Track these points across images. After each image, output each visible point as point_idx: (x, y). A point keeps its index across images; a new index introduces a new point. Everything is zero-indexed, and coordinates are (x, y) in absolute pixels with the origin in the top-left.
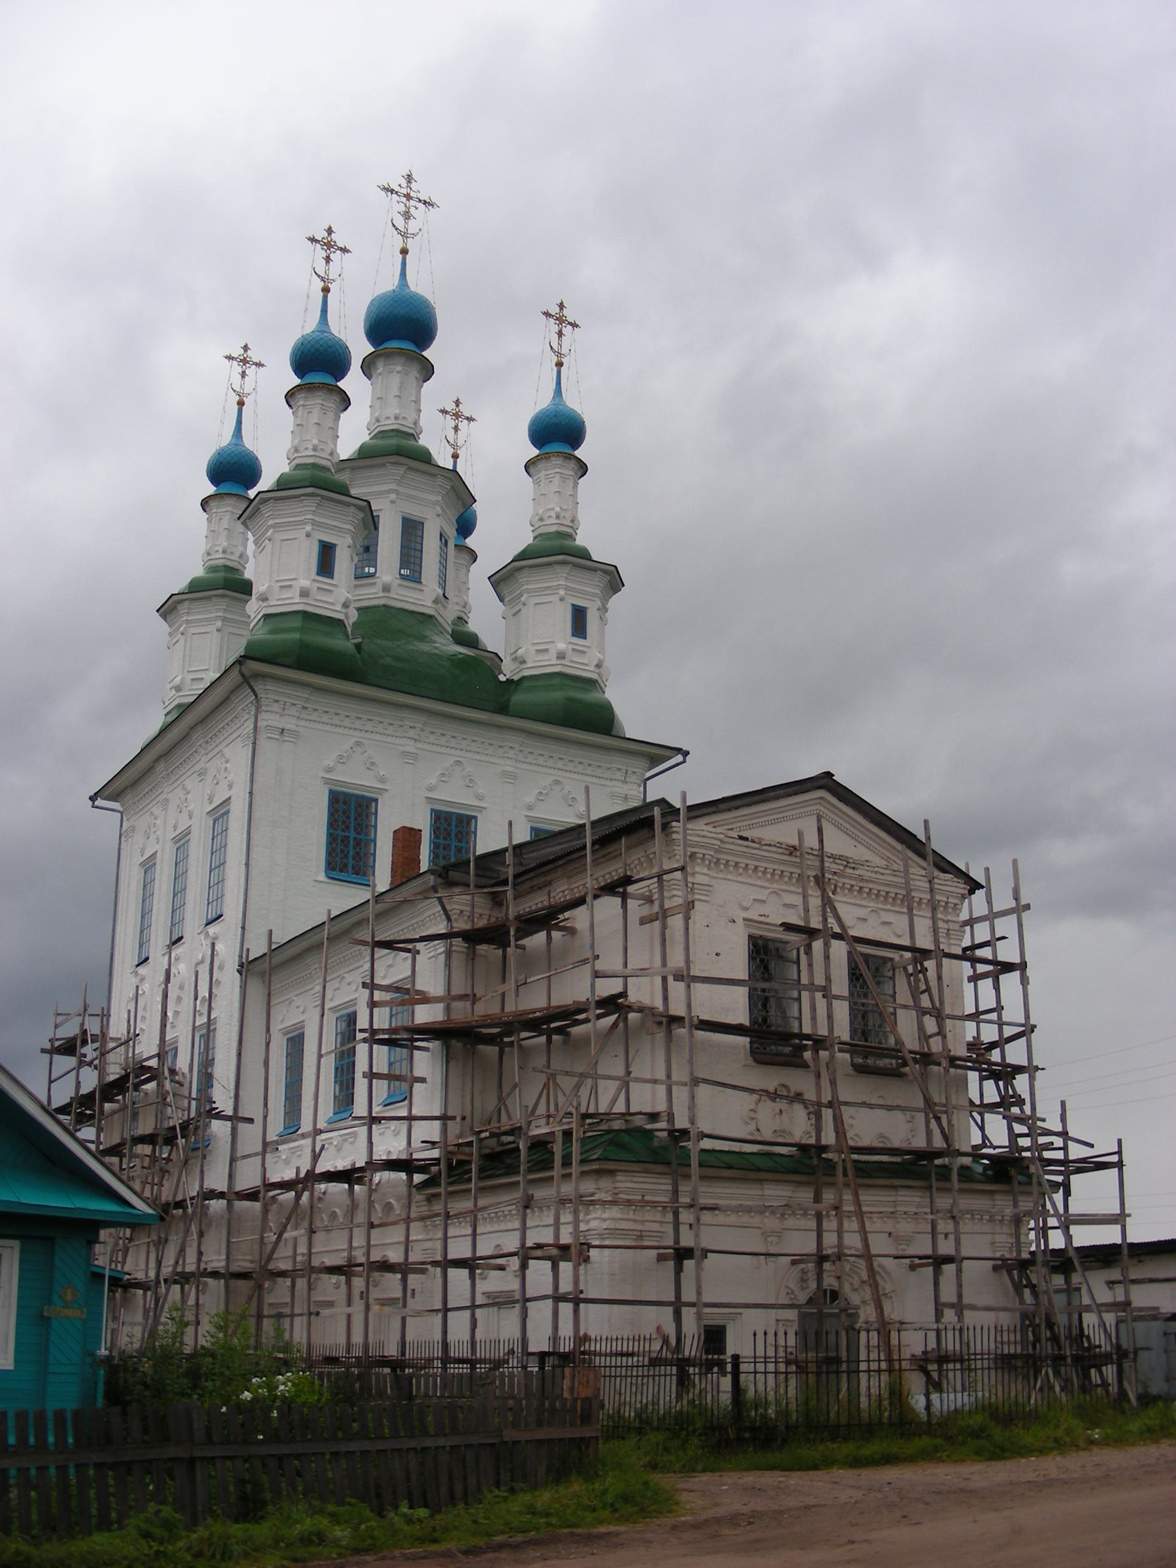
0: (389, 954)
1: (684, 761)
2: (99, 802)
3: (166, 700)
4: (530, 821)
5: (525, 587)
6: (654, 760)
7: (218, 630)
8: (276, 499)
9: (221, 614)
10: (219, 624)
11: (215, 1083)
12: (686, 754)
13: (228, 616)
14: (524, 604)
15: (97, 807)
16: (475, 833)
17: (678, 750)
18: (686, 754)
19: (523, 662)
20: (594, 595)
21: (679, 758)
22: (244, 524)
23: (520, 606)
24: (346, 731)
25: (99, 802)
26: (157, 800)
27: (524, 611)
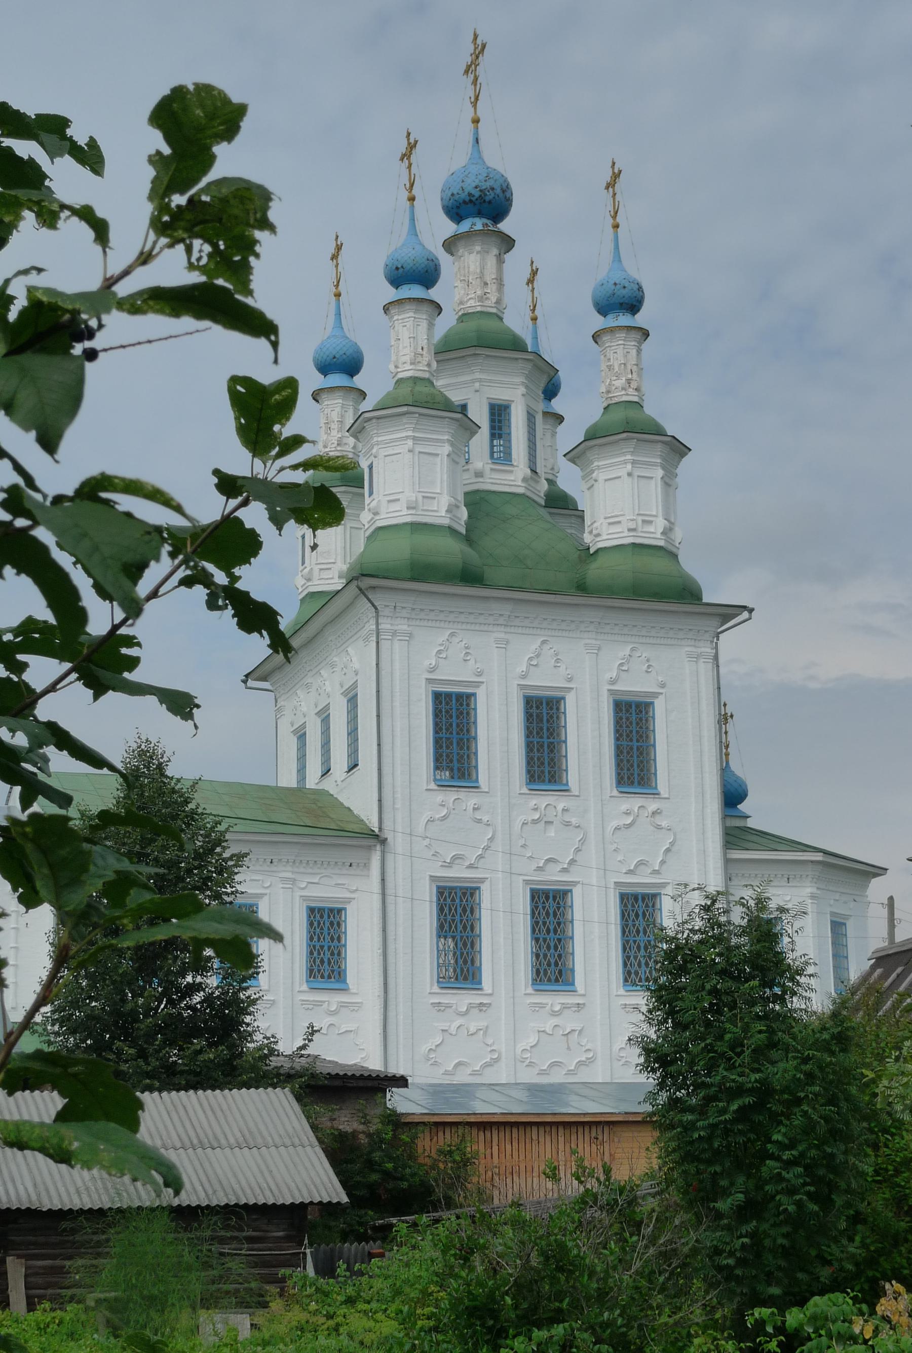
0: (50, 1116)
1: (750, 619)
2: (251, 683)
3: (299, 587)
4: (304, 900)
5: (596, 464)
6: (726, 618)
7: (409, 451)
8: (378, 418)
9: (410, 433)
10: (410, 443)
11: (172, 1156)
12: (751, 611)
13: (417, 435)
14: (596, 481)
15: (251, 688)
16: (565, 727)
17: (744, 608)
18: (751, 611)
19: (598, 535)
20: (654, 464)
21: (745, 615)
22: (356, 437)
23: (592, 482)
24: (442, 624)
25: (251, 683)
26: (358, 635)
27: (596, 484)
